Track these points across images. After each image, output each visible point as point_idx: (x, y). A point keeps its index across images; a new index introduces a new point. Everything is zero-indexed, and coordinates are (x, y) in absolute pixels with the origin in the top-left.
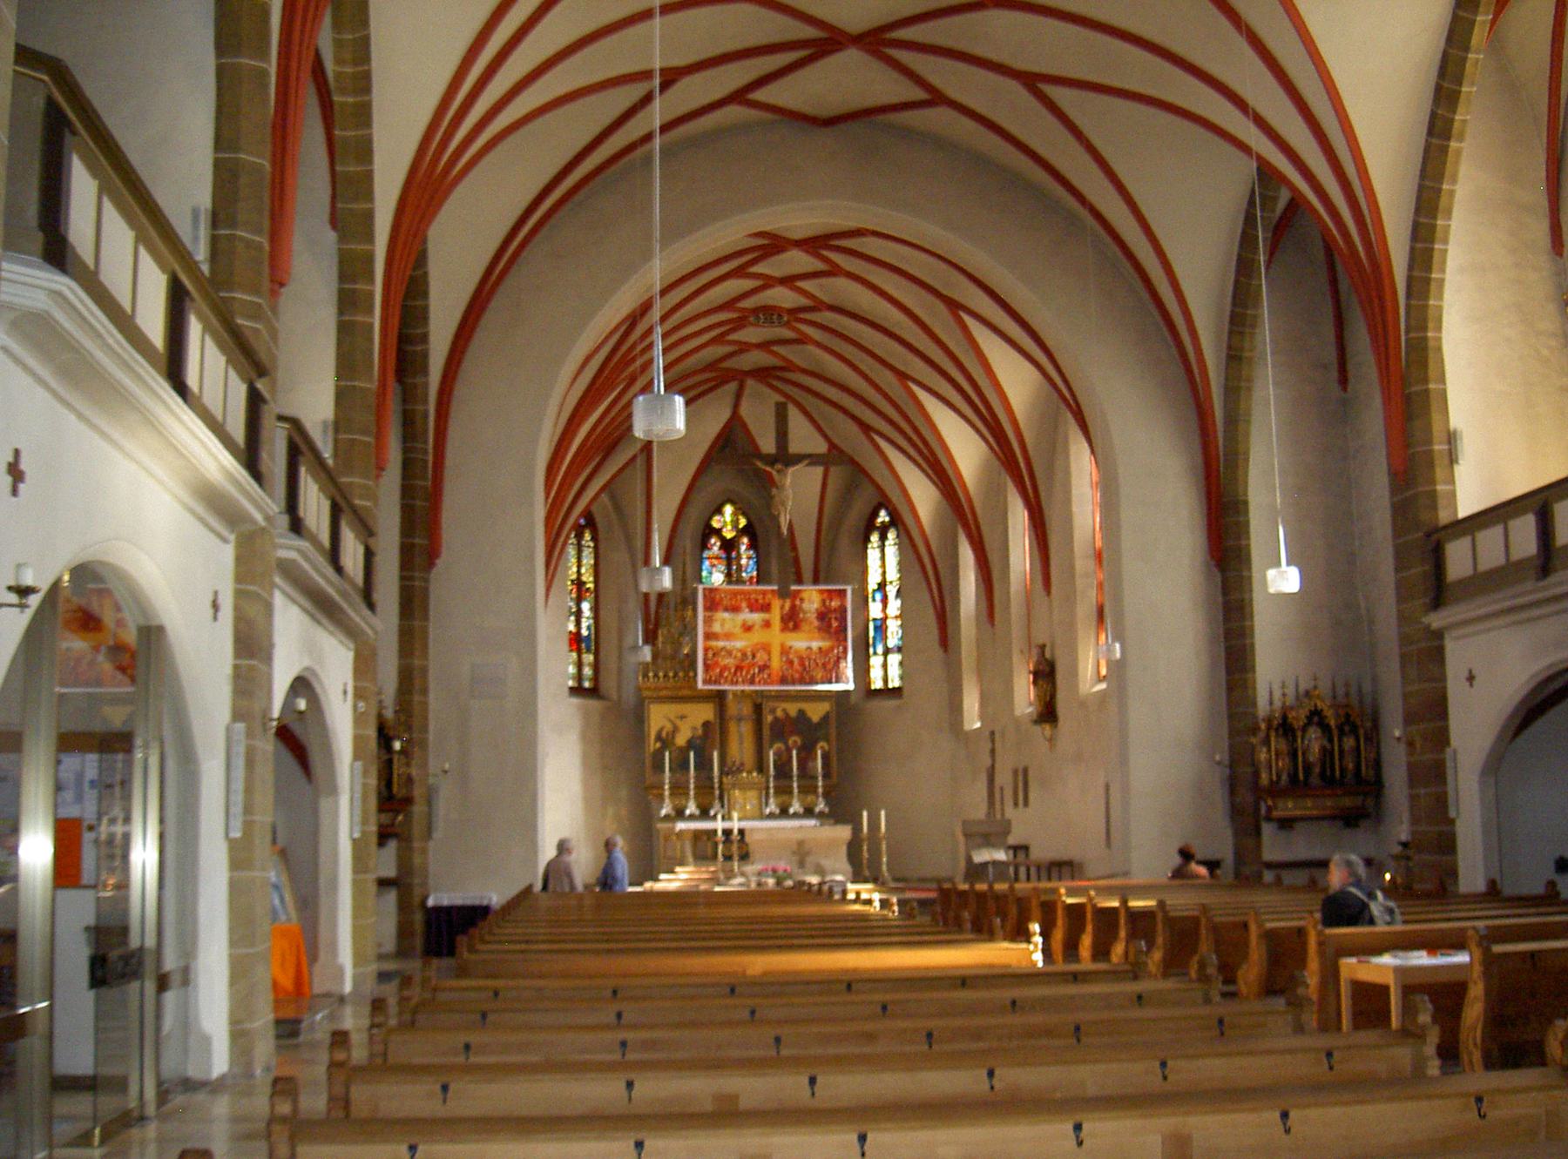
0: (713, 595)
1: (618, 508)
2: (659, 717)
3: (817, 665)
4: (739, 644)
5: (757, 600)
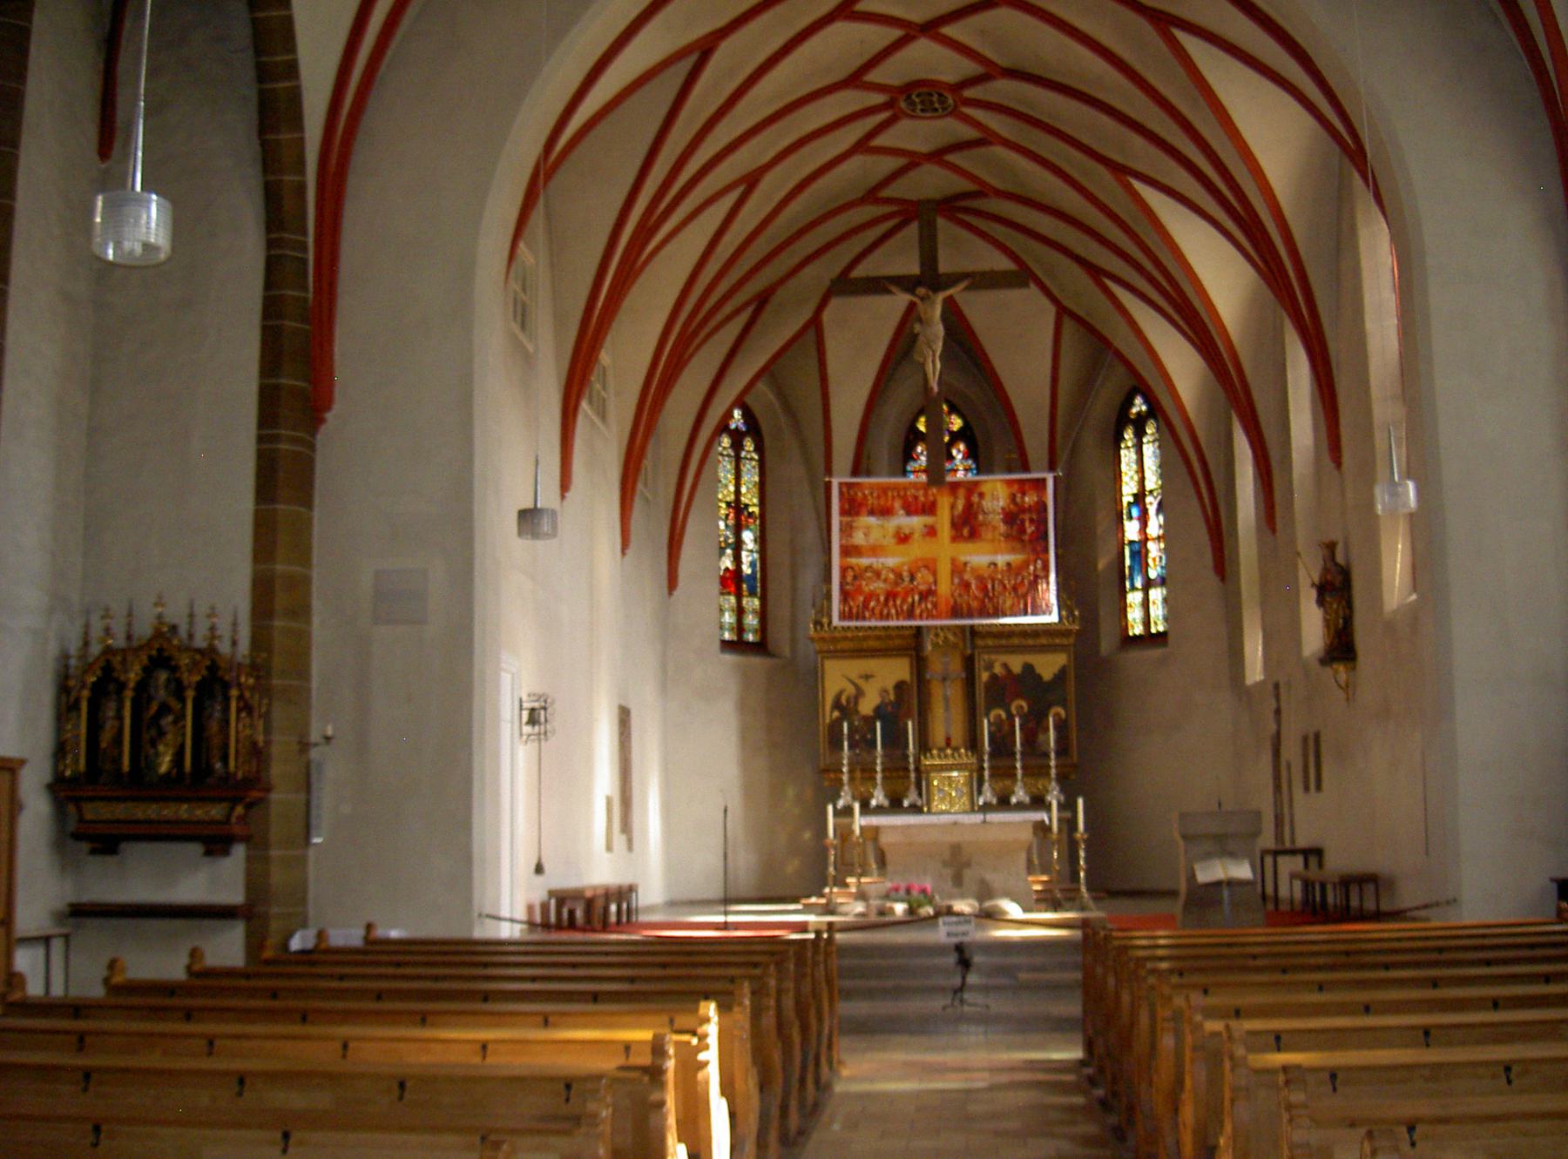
0: (852, 493)
1: (789, 409)
2: (837, 677)
3: (1005, 587)
4: (891, 562)
5: (916, 498)
